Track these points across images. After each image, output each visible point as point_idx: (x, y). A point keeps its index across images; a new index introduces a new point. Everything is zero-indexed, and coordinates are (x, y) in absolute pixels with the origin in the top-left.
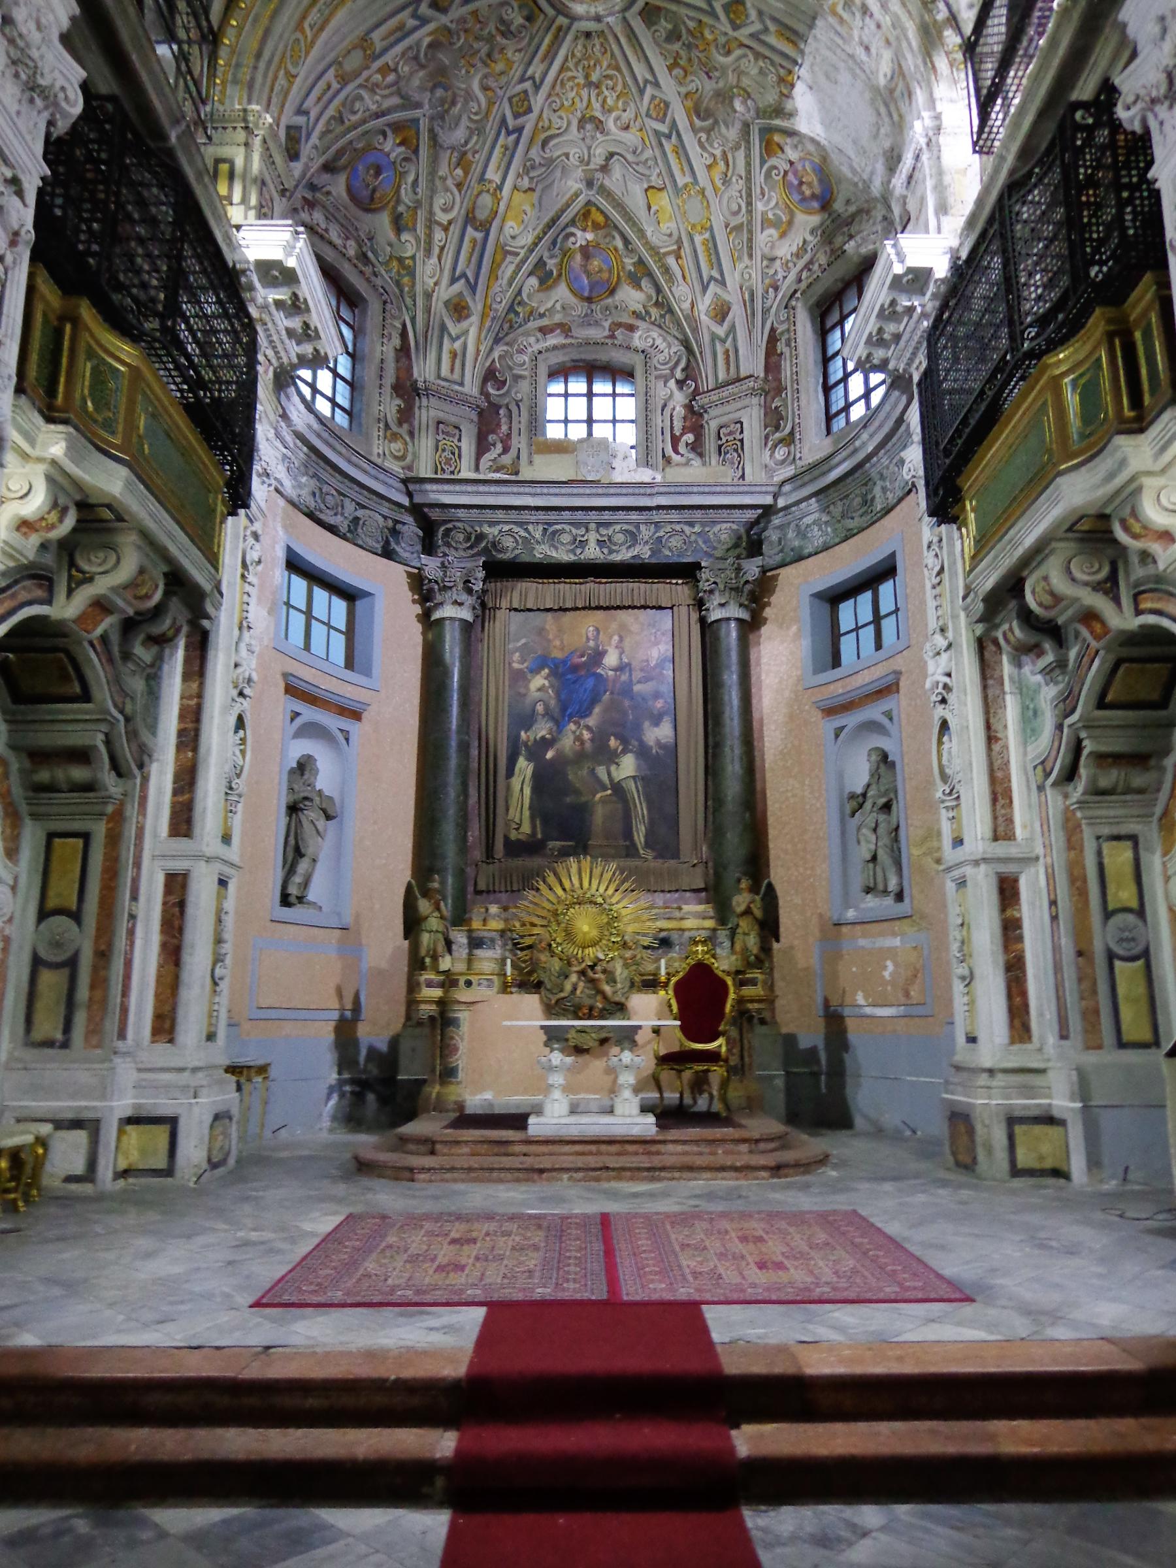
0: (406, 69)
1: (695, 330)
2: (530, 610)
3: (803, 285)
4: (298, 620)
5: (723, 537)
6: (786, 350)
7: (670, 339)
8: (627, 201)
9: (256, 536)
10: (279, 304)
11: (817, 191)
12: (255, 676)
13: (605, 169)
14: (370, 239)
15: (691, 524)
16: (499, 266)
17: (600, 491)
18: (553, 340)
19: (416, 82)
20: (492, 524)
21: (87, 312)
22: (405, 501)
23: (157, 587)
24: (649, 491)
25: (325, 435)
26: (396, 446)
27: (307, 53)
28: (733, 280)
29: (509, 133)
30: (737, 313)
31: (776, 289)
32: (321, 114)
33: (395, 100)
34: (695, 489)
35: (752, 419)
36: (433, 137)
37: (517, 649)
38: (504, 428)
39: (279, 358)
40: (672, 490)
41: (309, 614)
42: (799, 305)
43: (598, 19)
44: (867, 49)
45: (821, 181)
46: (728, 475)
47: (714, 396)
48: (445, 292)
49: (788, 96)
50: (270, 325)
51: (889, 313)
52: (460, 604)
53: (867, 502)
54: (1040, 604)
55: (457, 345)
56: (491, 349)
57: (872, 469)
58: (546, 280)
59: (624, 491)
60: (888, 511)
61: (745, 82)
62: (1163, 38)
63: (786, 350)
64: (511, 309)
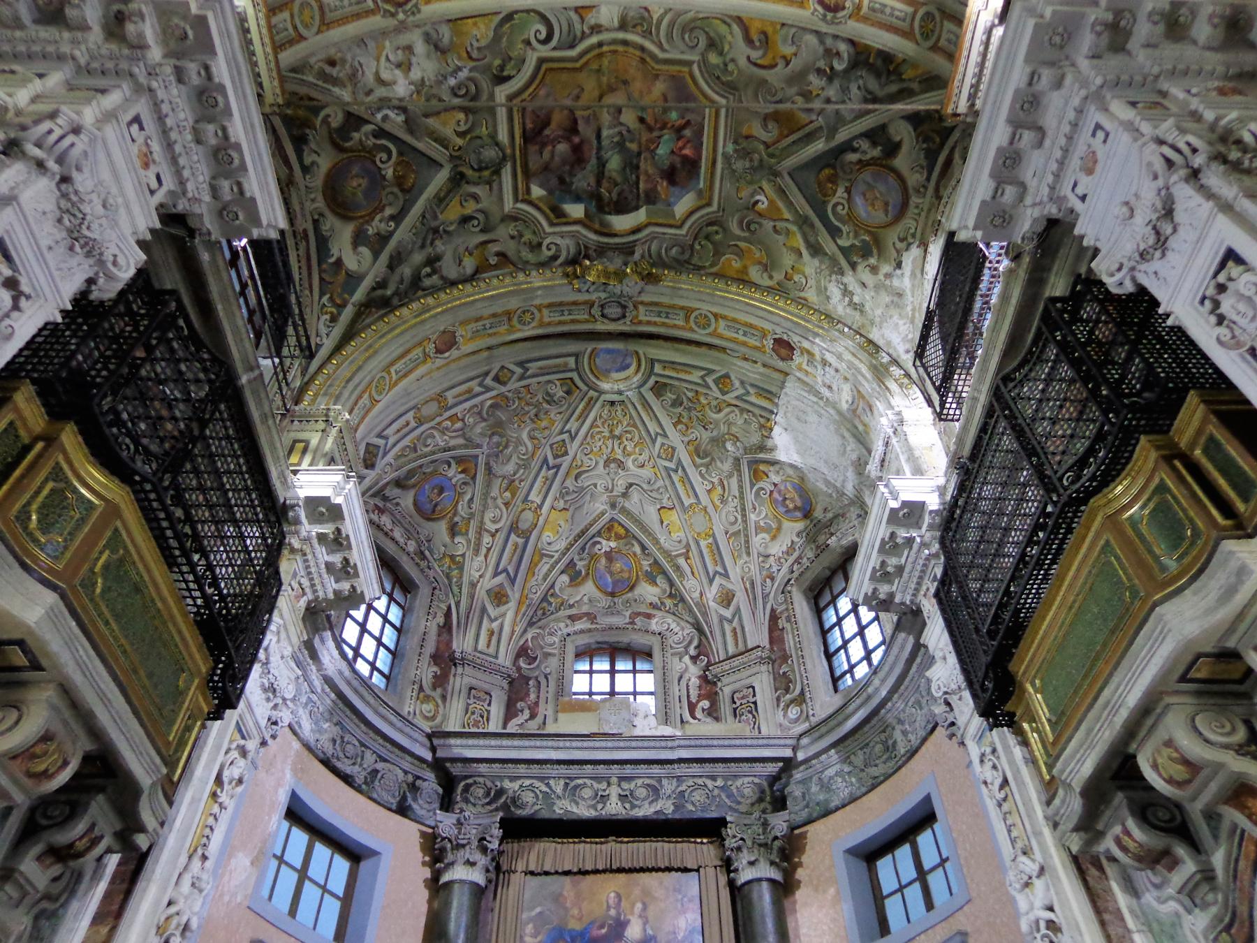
0: (471, 420)
1: (705, 614)
2: (547, 873)
3: (795, 575)
4: (288, 879)
5: (747, 791)
6: (787, 626)
7: (683, 624)
8: (643, 518)
9: (243, 752)
10: (322, 538)
11: (799, 504)
12: (194, 924)
13: (625, 495)
14: (429, 541)
15: (713, 778)
16: (536, 565)
17: (622, 744)
18: (580, 625)
19: (478, 430)
20: (513, 779)
21: (70, 437)
22: (428, 756)
23: (65, 763)
24: (670, 744)
25: (355, 683)
26: (427, 708)
27: (390, 390)
28: (735, 572)
29: (549, 469)
30: (741, 599)
31: (773, 579)
32: (398, 442)
33: (461, 441)
34: (715, 742)
35: (763, 683)
36: (489, 469)
37: (531, 920)
38: (533, 696)
39: (315, 591)
40: (693, 743)
41: (303, 874)
42: (794, 589)
43: (620, 393)
44: (830, 387)
45: (800, 496)
46: (746, 730)
47: (726, 665)
48: (488, 583)
49: (769, 437)
50: (310, 557)
51: (891, 546)
52: (473, 864)
53: (889, 748)
54: (1170, 781)
55: (495, 625)
56: (525, 631)
57: (888, 715)
58: (576, 578)
59: (646, 744)
60: (913, 753)
61: (734, 430)
62: (1132, 216)
63: (787, 626)
64: (544, 599)
